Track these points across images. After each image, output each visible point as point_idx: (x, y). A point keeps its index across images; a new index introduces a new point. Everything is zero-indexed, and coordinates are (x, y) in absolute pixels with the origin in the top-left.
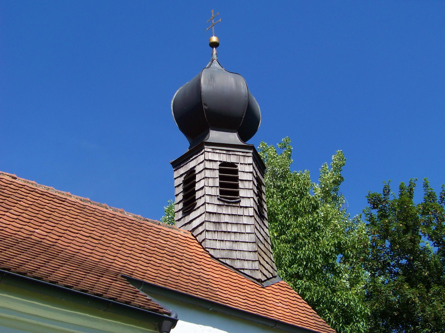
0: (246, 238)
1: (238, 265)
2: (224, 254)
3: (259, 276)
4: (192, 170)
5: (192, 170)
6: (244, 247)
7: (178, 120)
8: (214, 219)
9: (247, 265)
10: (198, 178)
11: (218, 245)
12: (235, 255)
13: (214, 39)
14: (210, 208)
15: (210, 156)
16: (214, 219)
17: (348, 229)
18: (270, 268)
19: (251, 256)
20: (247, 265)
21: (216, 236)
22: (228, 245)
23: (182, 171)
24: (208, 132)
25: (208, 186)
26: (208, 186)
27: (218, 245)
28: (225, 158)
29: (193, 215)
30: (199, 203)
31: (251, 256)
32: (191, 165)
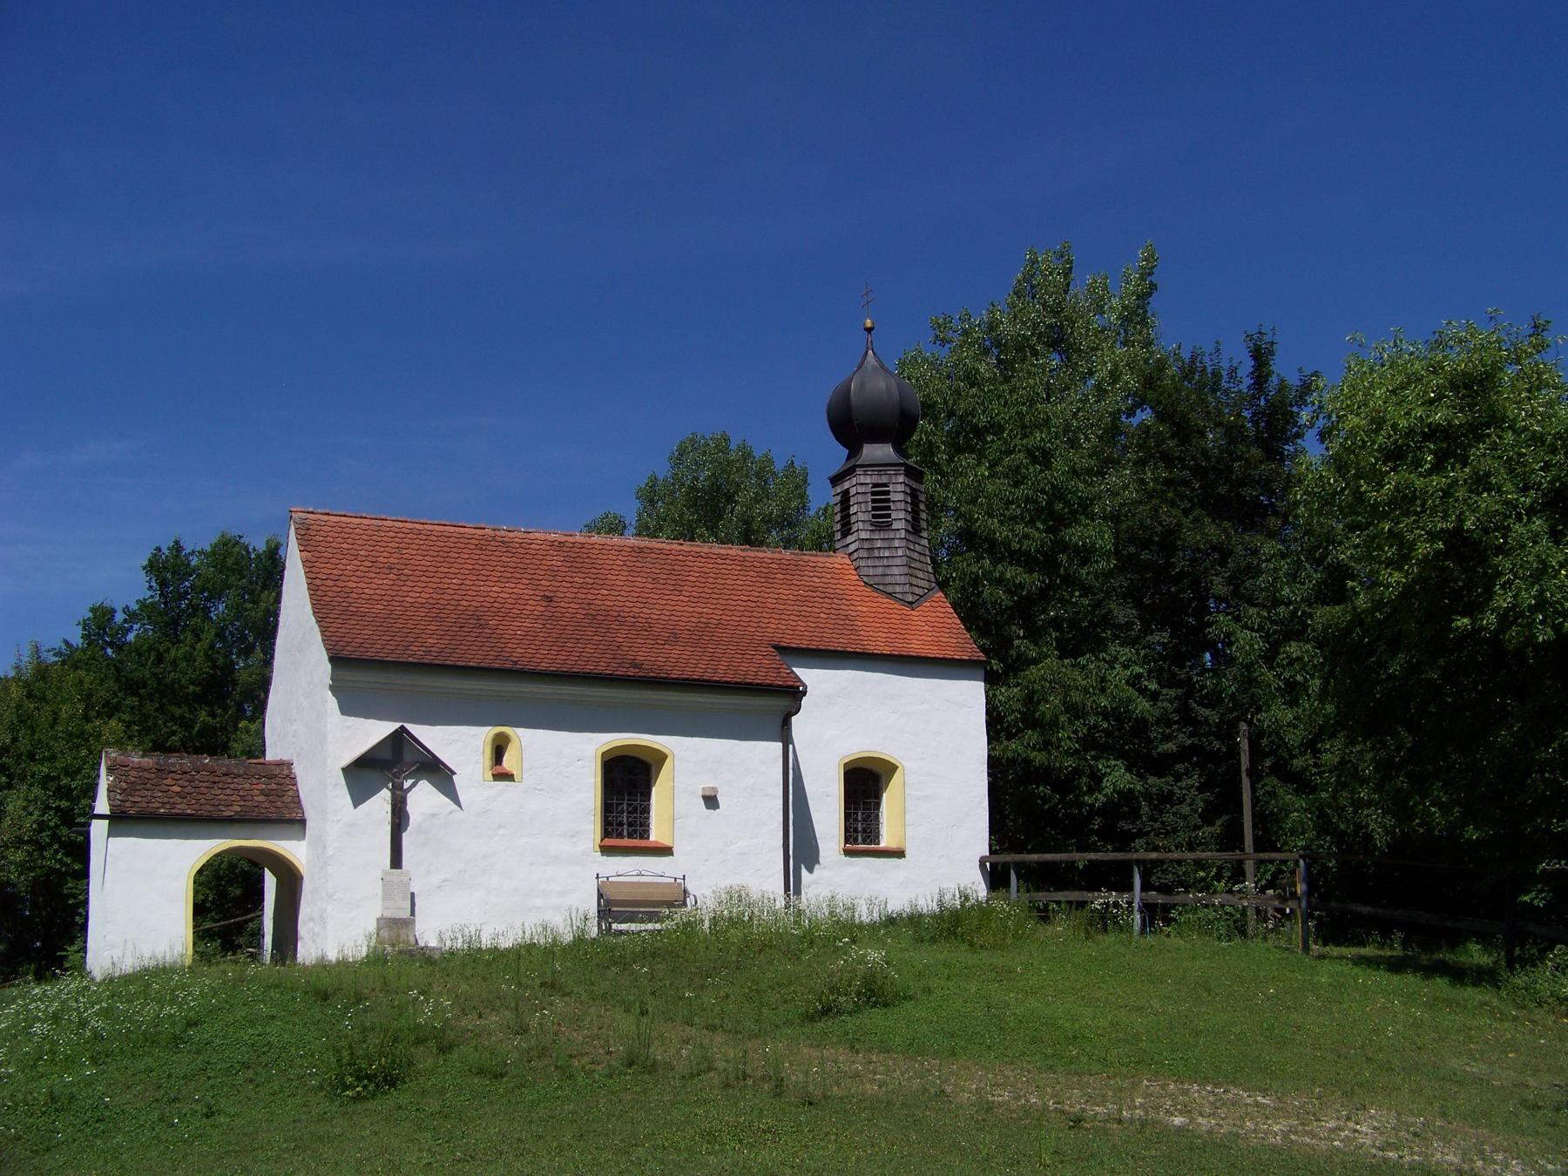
0: (898, 561)
1: (890, 589)
2: (877, 580)
3: (910, 598)
4: (846, 492)
5: (846, 492)
6: (895, 571)
7: (833, 430)
8: (866, 546)
9: (898, 589)
10: (852, 501)
11: (871, 571)
12: (888, 580)
13: (869, 323)
14: (864, 535)
15: (862, 479)
16: (866, 546)
17: (996, 1131)
18: (924, 579)
19: (902, 580)
20: (898, 589)
21: (870, 563)
22: (880, 571)
23: (839, 490)
24: (861, 448)
25: (861, 513)
26: (861, 513)
27: (871, 571)
28: (876, 480)
29: (850, 539)
30: (855, 528)
31: (902, 580)
32: (846, 485)
